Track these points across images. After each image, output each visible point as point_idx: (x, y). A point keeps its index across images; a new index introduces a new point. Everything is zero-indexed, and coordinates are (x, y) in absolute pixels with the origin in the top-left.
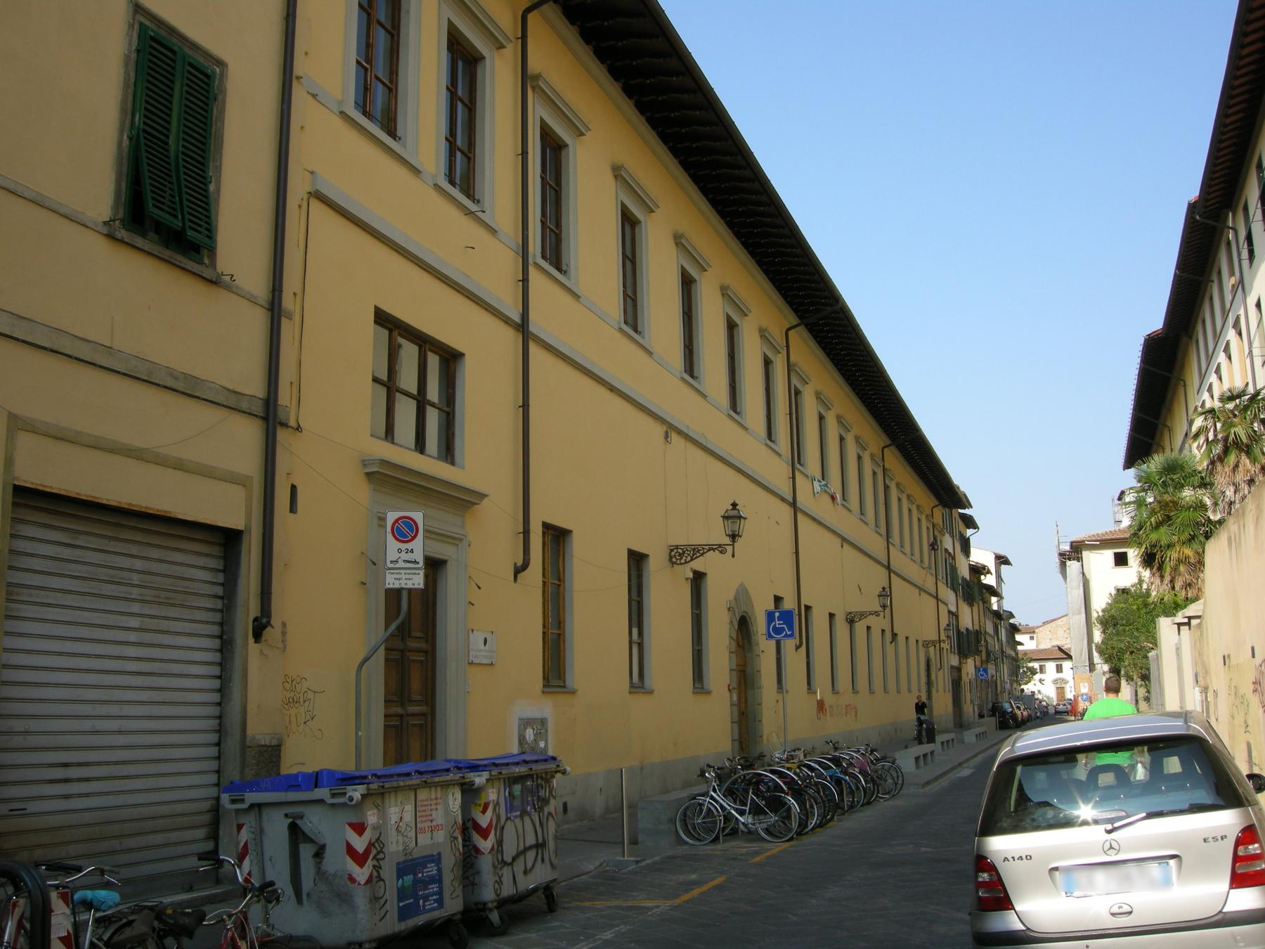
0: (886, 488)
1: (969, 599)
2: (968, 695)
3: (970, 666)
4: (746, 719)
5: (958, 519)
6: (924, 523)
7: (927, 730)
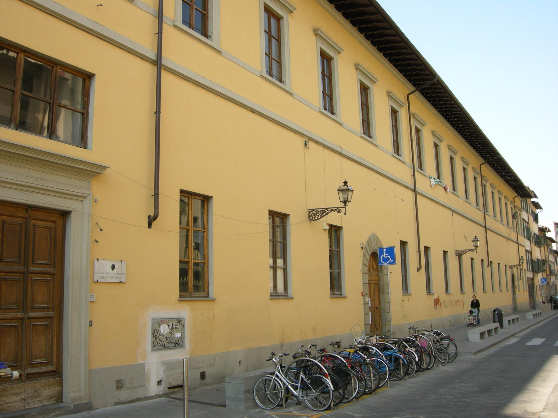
0: (484, 187)
1: (539, 244)
2: (539, 292)
4: (514, 300)
5: (530, 203)
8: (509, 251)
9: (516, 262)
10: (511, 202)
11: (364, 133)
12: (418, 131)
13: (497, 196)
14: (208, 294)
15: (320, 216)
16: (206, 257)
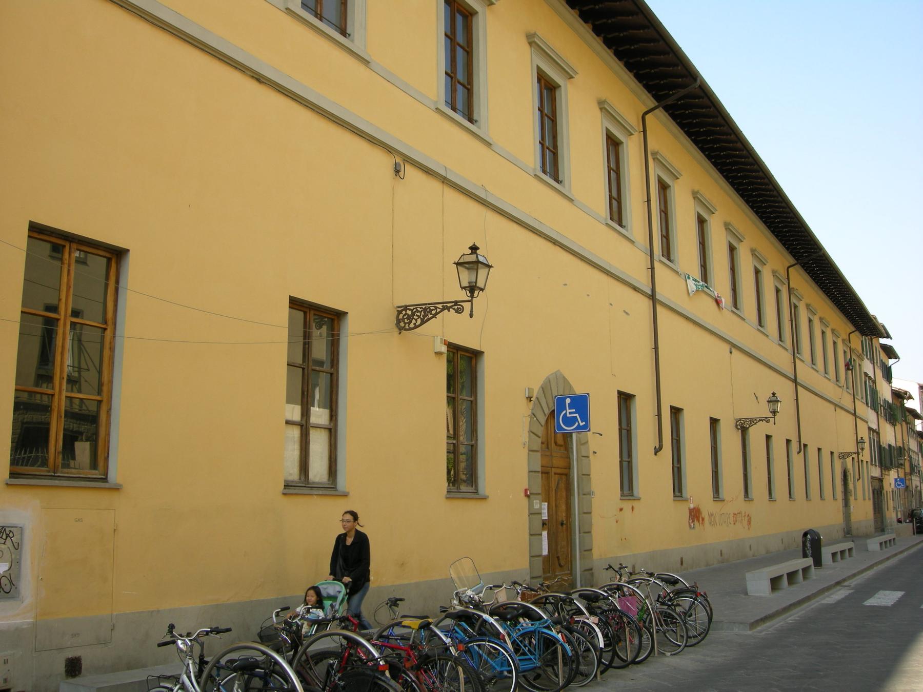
0: (794, 308)
2: (891, 503)
3: (893, 475)
5: (879, 349)
6: (841, 347)
7: (812, 540)
8: (837, 428)
9: (852, 448)
10: (843, 340)
11: (611, 219)
12: (663, 187)
13: (830, 338)
14: (106, 474)
15: (419, 321)
16: (105, 388)
